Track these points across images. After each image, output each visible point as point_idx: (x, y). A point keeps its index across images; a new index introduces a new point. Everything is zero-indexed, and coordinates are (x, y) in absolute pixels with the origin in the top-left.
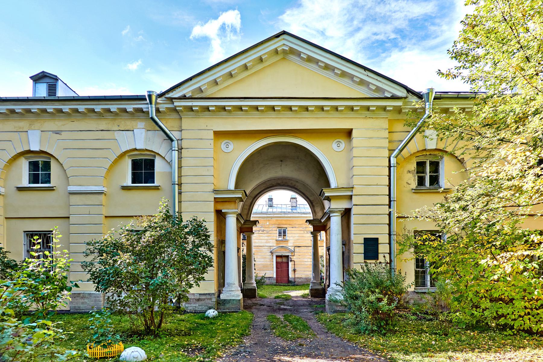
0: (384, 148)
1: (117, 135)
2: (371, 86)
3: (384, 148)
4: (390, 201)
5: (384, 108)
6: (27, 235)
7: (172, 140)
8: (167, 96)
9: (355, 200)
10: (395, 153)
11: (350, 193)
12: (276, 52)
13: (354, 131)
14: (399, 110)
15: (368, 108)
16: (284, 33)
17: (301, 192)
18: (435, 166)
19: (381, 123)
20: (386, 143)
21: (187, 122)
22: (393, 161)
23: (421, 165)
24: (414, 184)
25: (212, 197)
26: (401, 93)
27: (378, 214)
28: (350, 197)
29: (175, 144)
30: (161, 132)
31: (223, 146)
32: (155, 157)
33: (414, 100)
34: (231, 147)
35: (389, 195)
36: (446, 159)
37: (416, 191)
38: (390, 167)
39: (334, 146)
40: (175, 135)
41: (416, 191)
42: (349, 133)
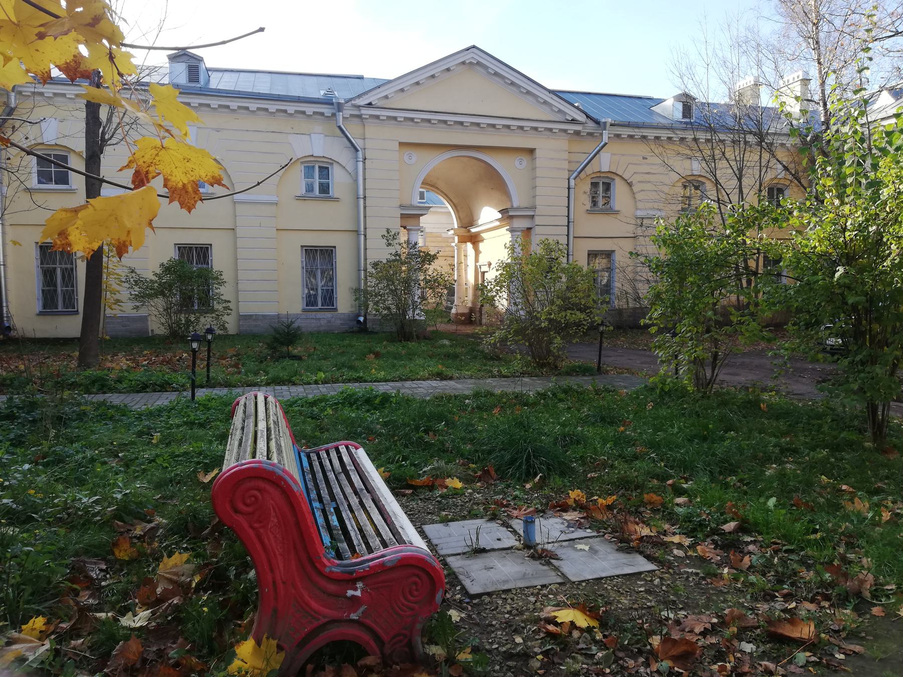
0: (563, 169)
1: (291, 138)
2: (554, 109)
3: (563, 169)
4: (569, 222)
5: (565, 131)
6: (179, 248)
7: (357, 150)
8: (353, 102)
9: (538, 220)
10: (575, 175)
11: (532, 213)
12: (463, 63)
13: (537, 151)
14: (577, 133)
15: (550, 130)
16: (474, 47)
17: (442, 192)
18: (607, 187)
19: (562, 143)
20: (566, 165)
21: (372, 130)
22: (572, 183)
23: (594, 185)
24: (588, 205)
25: (398, 212)
26: (581, 117)
27: (224, 43)
28: (532, 217)
29: (360, 154)
30: (345, 139)
31: (406, 158)
32: (332, 164)
33: (591, 124)
34: (414, 159)
35: (568, 216)
36: (617, 179)
37: (589, 212)
38: (569, 188)
39: (517, 163)
40: (358, 143)
41: (589, 212)
42: (531, 151)
